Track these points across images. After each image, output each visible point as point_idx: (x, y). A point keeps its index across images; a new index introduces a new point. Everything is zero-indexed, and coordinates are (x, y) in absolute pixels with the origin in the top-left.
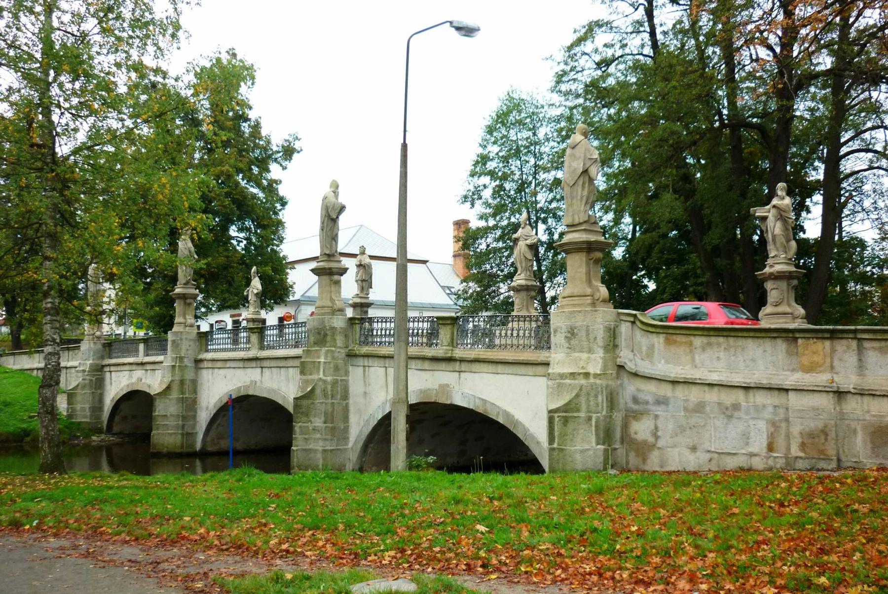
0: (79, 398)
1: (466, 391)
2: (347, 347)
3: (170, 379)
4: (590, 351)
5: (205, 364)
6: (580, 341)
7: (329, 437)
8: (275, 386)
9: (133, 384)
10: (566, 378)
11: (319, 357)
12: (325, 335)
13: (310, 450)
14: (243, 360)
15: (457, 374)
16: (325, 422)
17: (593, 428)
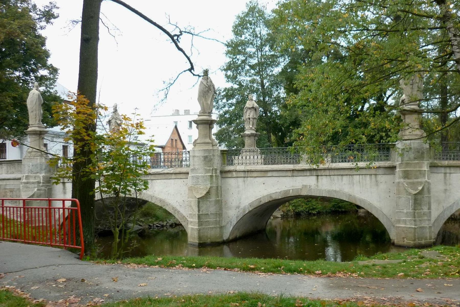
11: (421, 167)
12: (423, 153)
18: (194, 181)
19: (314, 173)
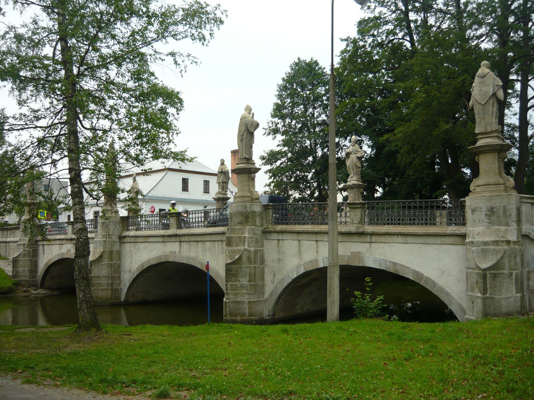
0: (20, 263)
1: (376, 256)
2: (262, 226)
3: (102, 251)
4: (507, 225)
5: (128, 240)
6: (498, 217)
7: (253, 292)
8: (193, 255)
9: (63, 254)
10: (490, 245)
11: (243, 233)
13: (239, 301)
14: (163, 236)
15: (368, 245)
16: (250, 281)
17: (514, 281)
18: (491, 256)
19: (178, 239)
